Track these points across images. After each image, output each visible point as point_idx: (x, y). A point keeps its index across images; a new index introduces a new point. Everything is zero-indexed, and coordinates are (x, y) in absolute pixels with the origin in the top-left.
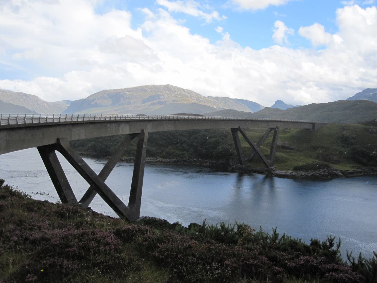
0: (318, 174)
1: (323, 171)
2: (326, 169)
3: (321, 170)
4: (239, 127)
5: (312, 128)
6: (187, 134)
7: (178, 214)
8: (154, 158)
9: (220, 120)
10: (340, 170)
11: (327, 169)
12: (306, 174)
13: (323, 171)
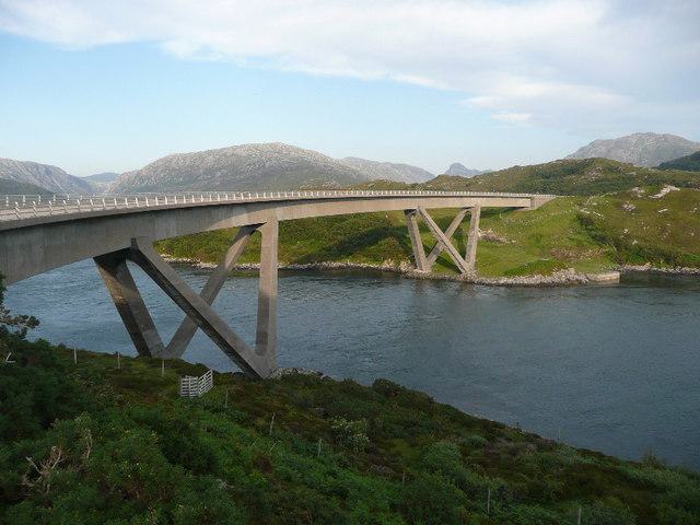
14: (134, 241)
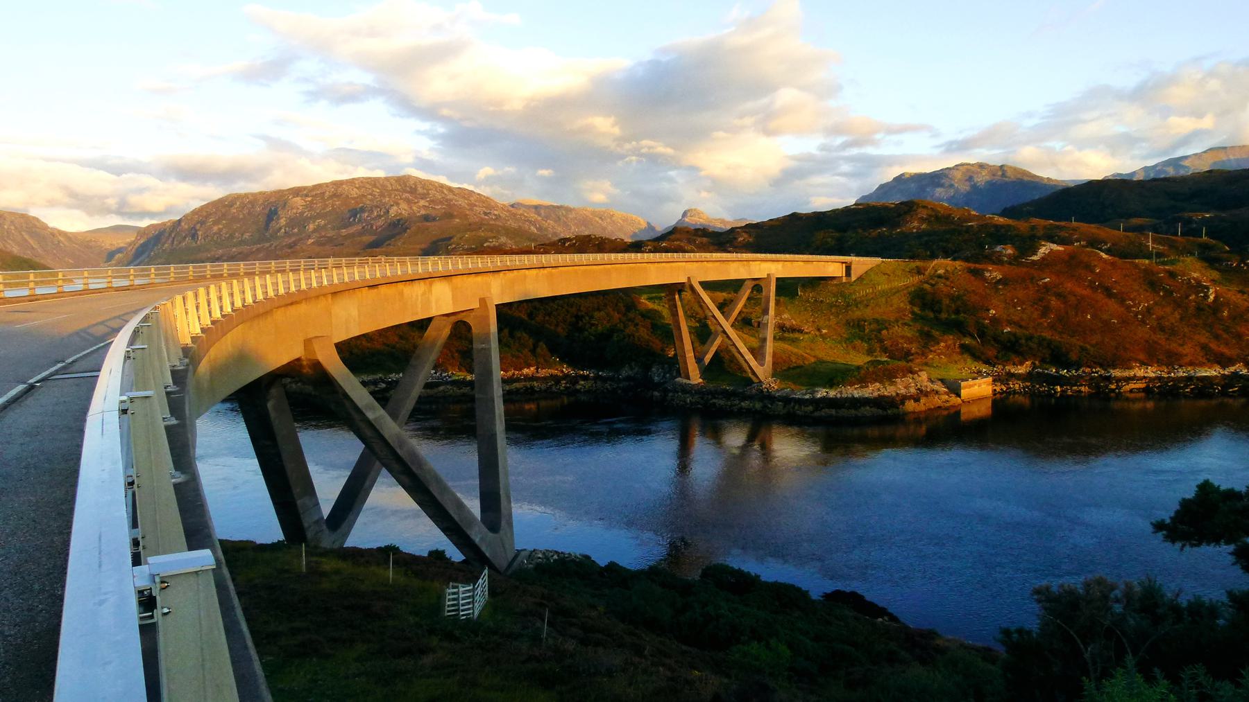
5: (844, 275)
14: (689, 278)
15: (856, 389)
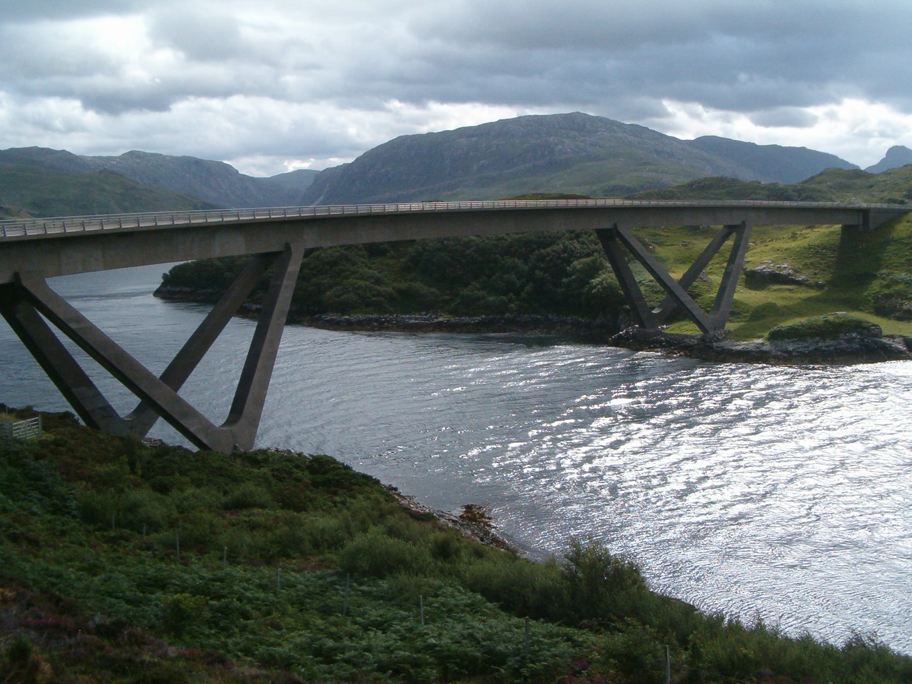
0: (832, 348)
1: (845, 340)
2: (854, 335)
3: (841, 335)
4: (615, 226)
6: (523, 249)
7: (307, 439)
8: (431, 316)
9: (773, 208)
10: (901, 336)
11: (859, 333)
12: (799, 348)
13: (845, 340)
15: (793, 342)
